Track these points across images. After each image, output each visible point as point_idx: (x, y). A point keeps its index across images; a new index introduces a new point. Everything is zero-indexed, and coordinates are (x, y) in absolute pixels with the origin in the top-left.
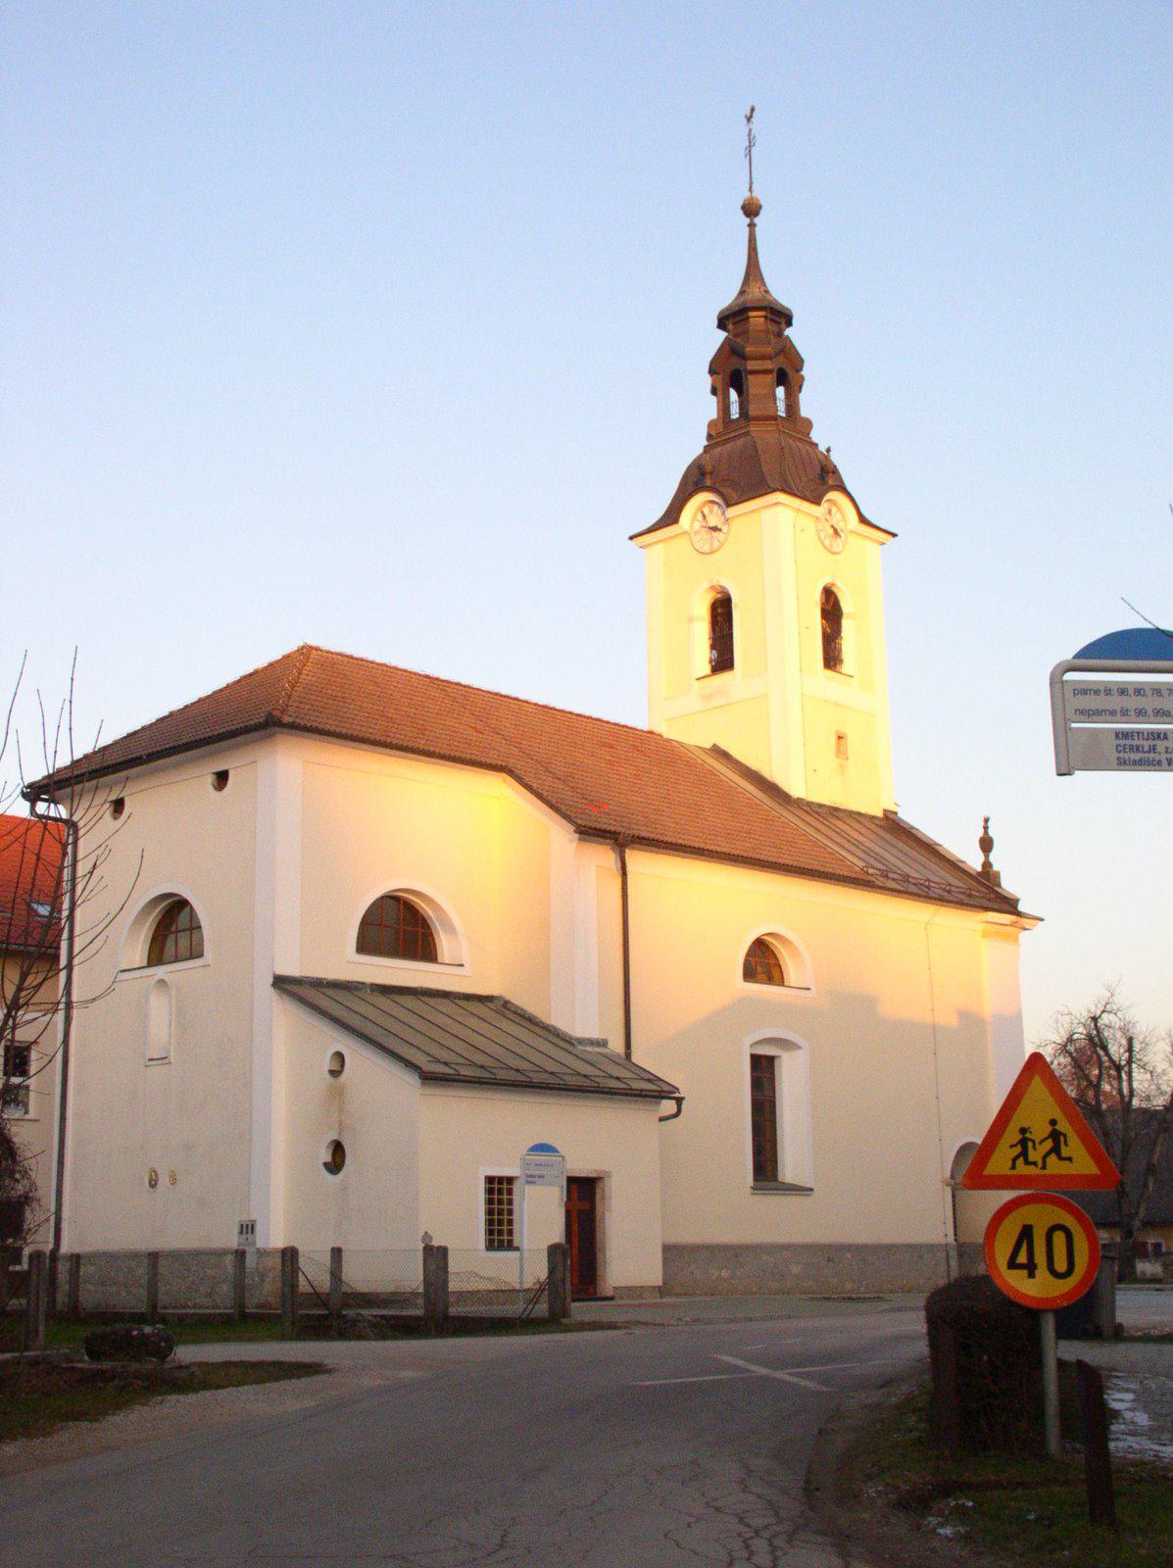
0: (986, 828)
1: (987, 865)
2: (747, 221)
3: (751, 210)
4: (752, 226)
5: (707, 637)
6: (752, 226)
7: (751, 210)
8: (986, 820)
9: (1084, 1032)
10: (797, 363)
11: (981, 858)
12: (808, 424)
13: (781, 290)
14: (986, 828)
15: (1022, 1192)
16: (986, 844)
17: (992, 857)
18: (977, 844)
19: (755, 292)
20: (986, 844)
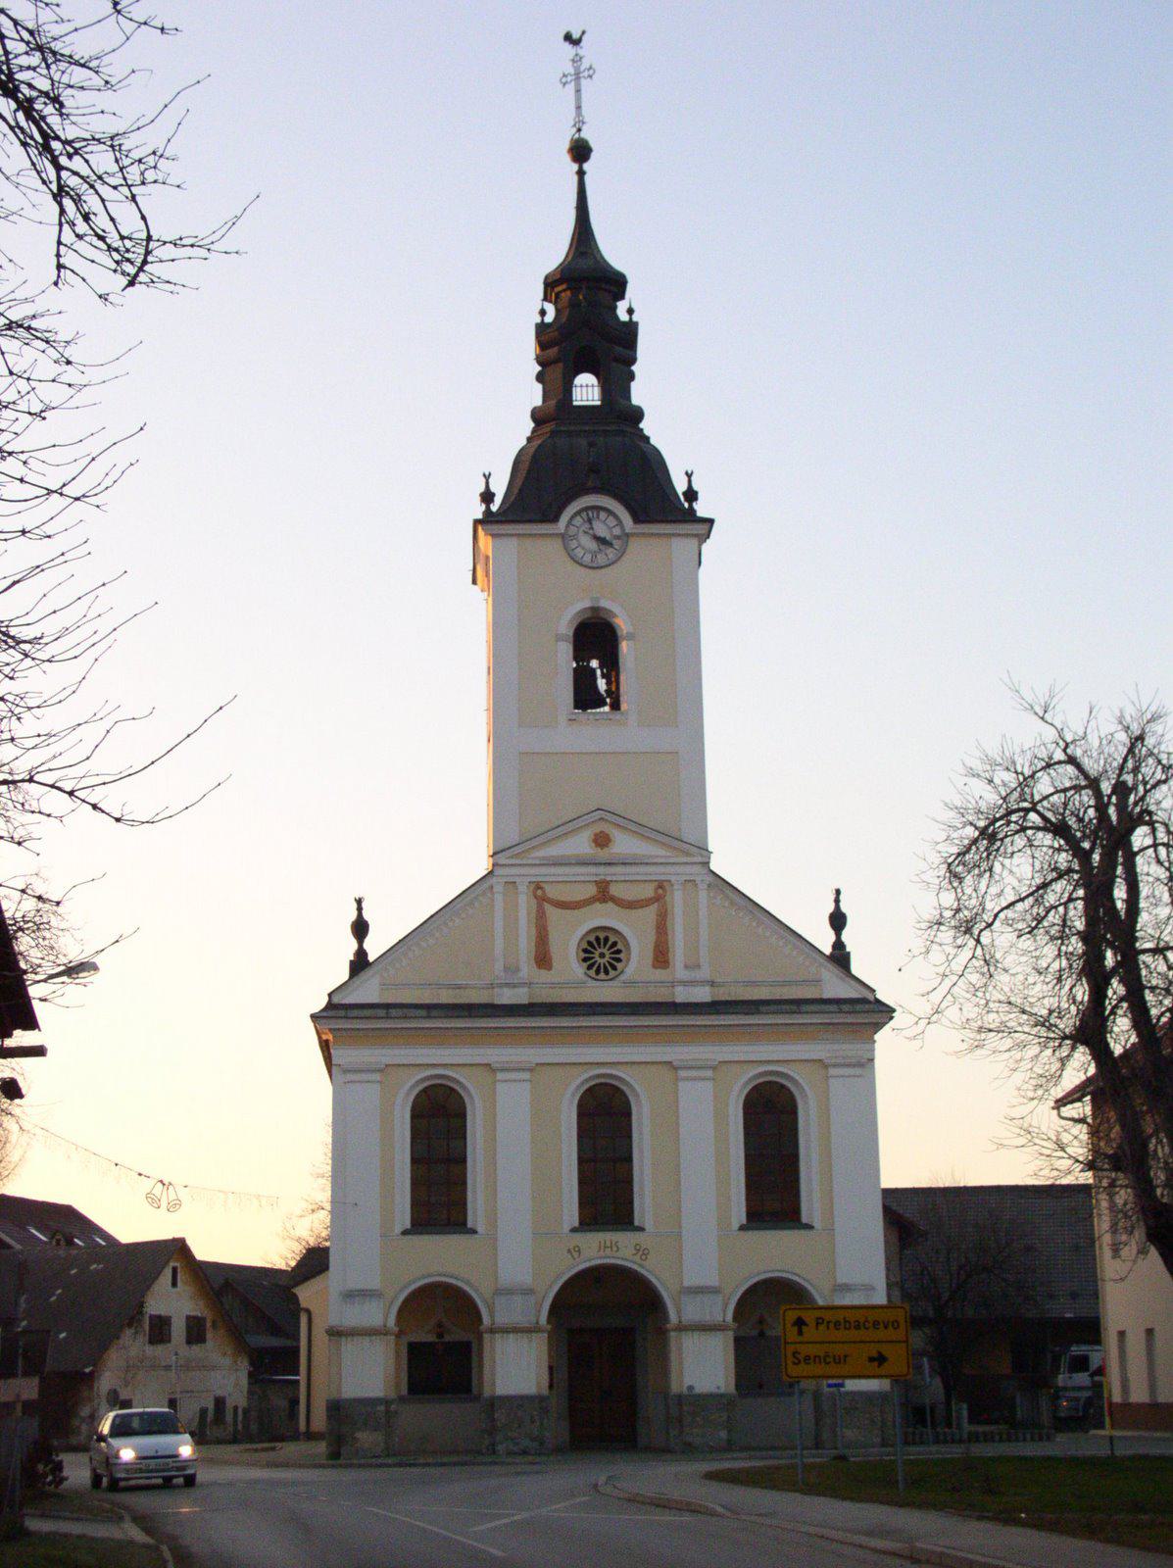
0: (837, 901)
1: (839, 945)
2: (575, 167)
3: (580, 152)
4: (581, 173)
5: (485, 639)
6: (581, 173)
7: (580, 152)
8: (838, 892)
9: (1036, 1049)
10: (627, 335)
11: (831, 937)
12: (637, 415)
13: (613, 250)
14: (837, 901)
15: (1119, 870)
16: (838, 921)
17: (845, 936)
18: (529, 414)
19: (586, 264)
20: (838, 921)
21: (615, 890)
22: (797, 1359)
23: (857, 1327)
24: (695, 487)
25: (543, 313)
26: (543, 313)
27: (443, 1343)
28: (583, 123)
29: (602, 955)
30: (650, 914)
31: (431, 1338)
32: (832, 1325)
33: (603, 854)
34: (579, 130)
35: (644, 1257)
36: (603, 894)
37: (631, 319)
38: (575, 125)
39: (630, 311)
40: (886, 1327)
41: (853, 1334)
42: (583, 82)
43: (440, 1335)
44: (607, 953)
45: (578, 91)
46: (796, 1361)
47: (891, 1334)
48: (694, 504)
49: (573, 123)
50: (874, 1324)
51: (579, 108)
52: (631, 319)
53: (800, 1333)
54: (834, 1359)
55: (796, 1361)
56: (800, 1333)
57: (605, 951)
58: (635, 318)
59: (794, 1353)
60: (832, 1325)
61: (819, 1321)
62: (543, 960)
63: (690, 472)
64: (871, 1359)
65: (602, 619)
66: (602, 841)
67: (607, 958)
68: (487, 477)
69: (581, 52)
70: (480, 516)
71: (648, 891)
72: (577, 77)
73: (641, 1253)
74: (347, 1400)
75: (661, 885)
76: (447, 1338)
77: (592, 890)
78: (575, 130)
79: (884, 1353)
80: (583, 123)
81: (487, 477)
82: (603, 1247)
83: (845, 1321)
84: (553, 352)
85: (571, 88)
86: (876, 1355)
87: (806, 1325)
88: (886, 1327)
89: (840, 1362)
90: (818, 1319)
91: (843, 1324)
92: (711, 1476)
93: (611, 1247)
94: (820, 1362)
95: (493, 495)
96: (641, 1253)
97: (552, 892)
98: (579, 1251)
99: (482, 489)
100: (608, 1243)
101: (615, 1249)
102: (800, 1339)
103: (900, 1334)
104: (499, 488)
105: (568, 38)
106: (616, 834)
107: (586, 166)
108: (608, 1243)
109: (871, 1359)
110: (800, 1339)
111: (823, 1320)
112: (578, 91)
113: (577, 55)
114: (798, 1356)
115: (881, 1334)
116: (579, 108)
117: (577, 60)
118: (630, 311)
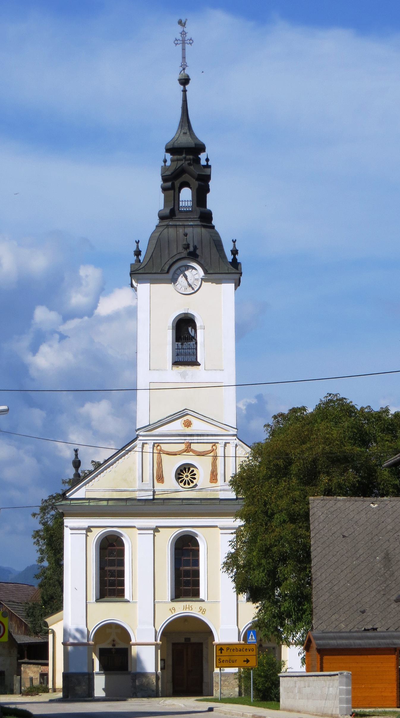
2: (182, 87)
3: (185, 81)
4: (185, 91)
6: (185, 91)
21: (193, 446)
22: (220, 661)
23: (240, 651)
24: (237, 248)
25: (165, 161)
26: (165, 161)
27: (115, 648)
28: (186, 66)
29: (187, 476)
30: (208, 460)
31: (110, 646)
32: (232, 650)
33: (188, 431)
34: (184, 69)
35: (203, 613)
36: (188, 449)
37: (207, 164)
38: (181, 66)
39: (207, 160)
40: (250, 651)
41: (239, 653)
42: (187, 46)
43: (114, 645)
44: (187, 479)
45: (184, 49)
46: (220, 662)
47: (251, 653)
48: (236, 256)
49: (180, 65)
50: (246, 650)
51: (184, 58)
52: (207, 164)
53: (221, 653)
54: (232, 661)
55: (220, 662)
56: (221, 653)
57: (188, 474)
58: (209, 163)
59: (219, 659)
60: (232, 650)
61: (228, 649)
62: (160, 478)
63: (234, 240)
64: (244, 661)
65: (189, 317)
66: (188, 424)
67: (189, 478)
68: (138, 242)
69: (185, 30)
70: (134, 262)
71: (209, 447)
72: (184, 42)
73: (202, 610)
74: (149, 672)
75: (215, 444)
76: (117, 646)
77: (183, 447)
78: (181, 69)
79: (248, 659)
80: (186, 66)
81: (138, 242)
82: (185, 608)
83: (236, 649)
84: (169, 184)
85: (180, 47)
86: (246, 660)
87: (223, 650)
88: (250, 651)
89: (234, 662)
90: (227, 648)
91: (235, 650)
92: (197, 700)
93: (189, 608)
94: (227, 662)
95: (140, 251)
96: (202, 610)
97: (165, 447)
98: (175, 609)
99: (135, 248)
100: (188, 607)
101: (190, 609)
102: (221, 655)
103: (254, 653)
104: (143, 248)
105: (180, 22)
106: (194, 421)
107: (187, 87)
108: (188, 607)
109: (244, 661)
110: (221, 655)
111: (229, 649)
112: (184, 49)
113: (183, 31)
114: (221, 660)
115: (248, 653)
116: (184, 58)
117: (184, 33)
118: (207, 160)
